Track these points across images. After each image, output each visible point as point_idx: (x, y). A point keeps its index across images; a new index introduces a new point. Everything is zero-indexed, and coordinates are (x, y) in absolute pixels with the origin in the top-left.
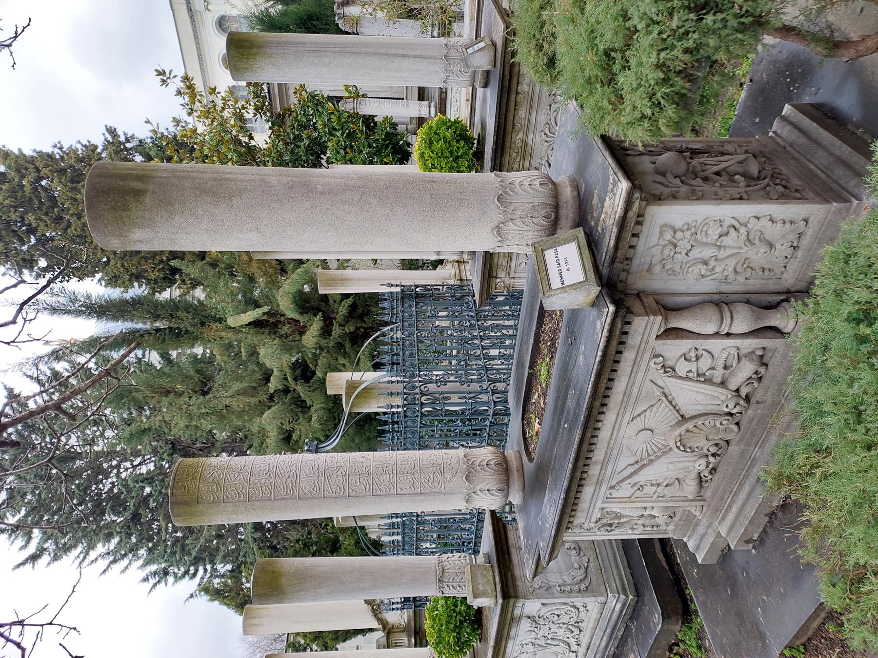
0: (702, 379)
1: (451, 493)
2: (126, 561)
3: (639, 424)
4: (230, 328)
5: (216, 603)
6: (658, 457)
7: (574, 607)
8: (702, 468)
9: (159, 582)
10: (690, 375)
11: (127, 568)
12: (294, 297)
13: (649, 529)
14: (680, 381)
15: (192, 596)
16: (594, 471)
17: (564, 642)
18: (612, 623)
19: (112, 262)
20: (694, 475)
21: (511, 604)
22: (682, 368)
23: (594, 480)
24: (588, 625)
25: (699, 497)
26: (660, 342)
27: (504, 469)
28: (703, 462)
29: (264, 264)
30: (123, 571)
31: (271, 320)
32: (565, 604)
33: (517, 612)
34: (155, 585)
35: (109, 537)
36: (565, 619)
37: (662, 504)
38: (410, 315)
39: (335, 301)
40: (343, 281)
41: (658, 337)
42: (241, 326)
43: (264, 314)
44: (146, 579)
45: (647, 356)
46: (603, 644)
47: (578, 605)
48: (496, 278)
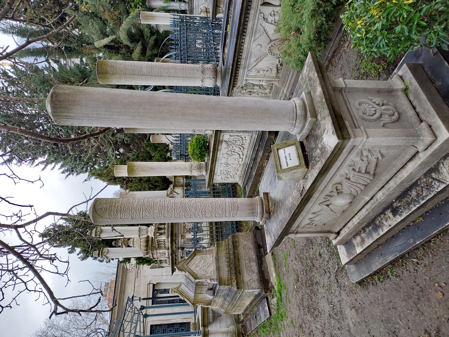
0: (276, 24)
1: (196, 78)
2: (53, 164)
3: (256, 42)
4: (96, 48)
5: (98, 179)
6: (263, 58)
7: (241, 137)
8: (278, 63)
9: (69, 174)
10: (272, 22)
11: (53, 168)
12: (128, 32)
13: (264, 95)
14: (269, 24)
15: (86, 180)
16: (243, 62)
17: (238, 153)
18: (254, 144)
19: (29, 11)
20: (275, 66)
21: (219, 134)
22: (270, 19)
23: (243, 66)
24: (246, 146)
25: (277, 77)
26: (262, 7)
27: (216, 71)
28: (278, 60)
29: (111, 14)
30: (52, 169)
31: (116, 46)
32: (238, 136)
33: (221, 138)
34: (68, 176)
35: (44, 153)
36: (238, 143)
37: (265, 79)
38: (183, 29)
39: (147, 37)
40: (153, 17)
41: (261, 5)
42: (101, 47)
43: (112, 41)
44: (63, 172)
45: (258, 12)
46: (251, 154)
47: (243, 137)
48: (219, 7)
